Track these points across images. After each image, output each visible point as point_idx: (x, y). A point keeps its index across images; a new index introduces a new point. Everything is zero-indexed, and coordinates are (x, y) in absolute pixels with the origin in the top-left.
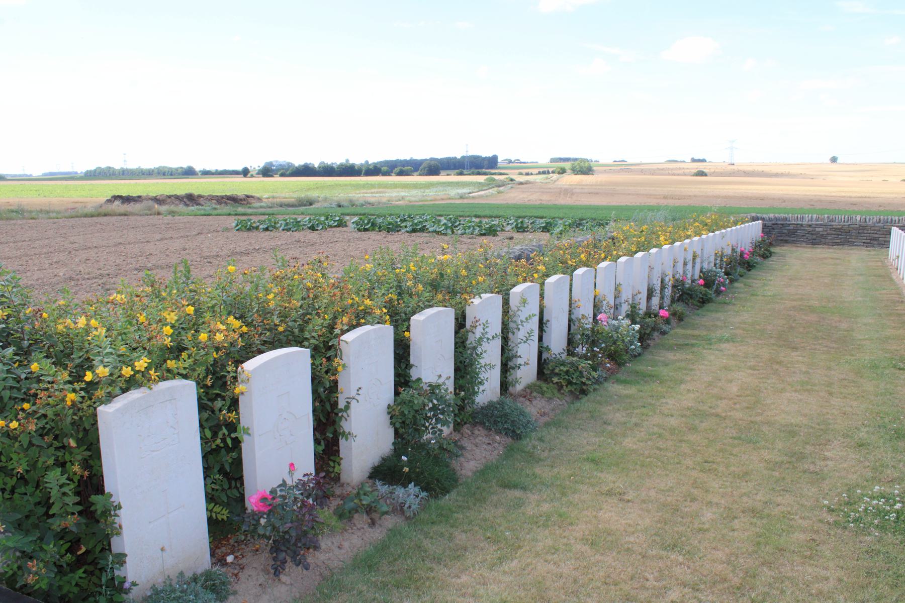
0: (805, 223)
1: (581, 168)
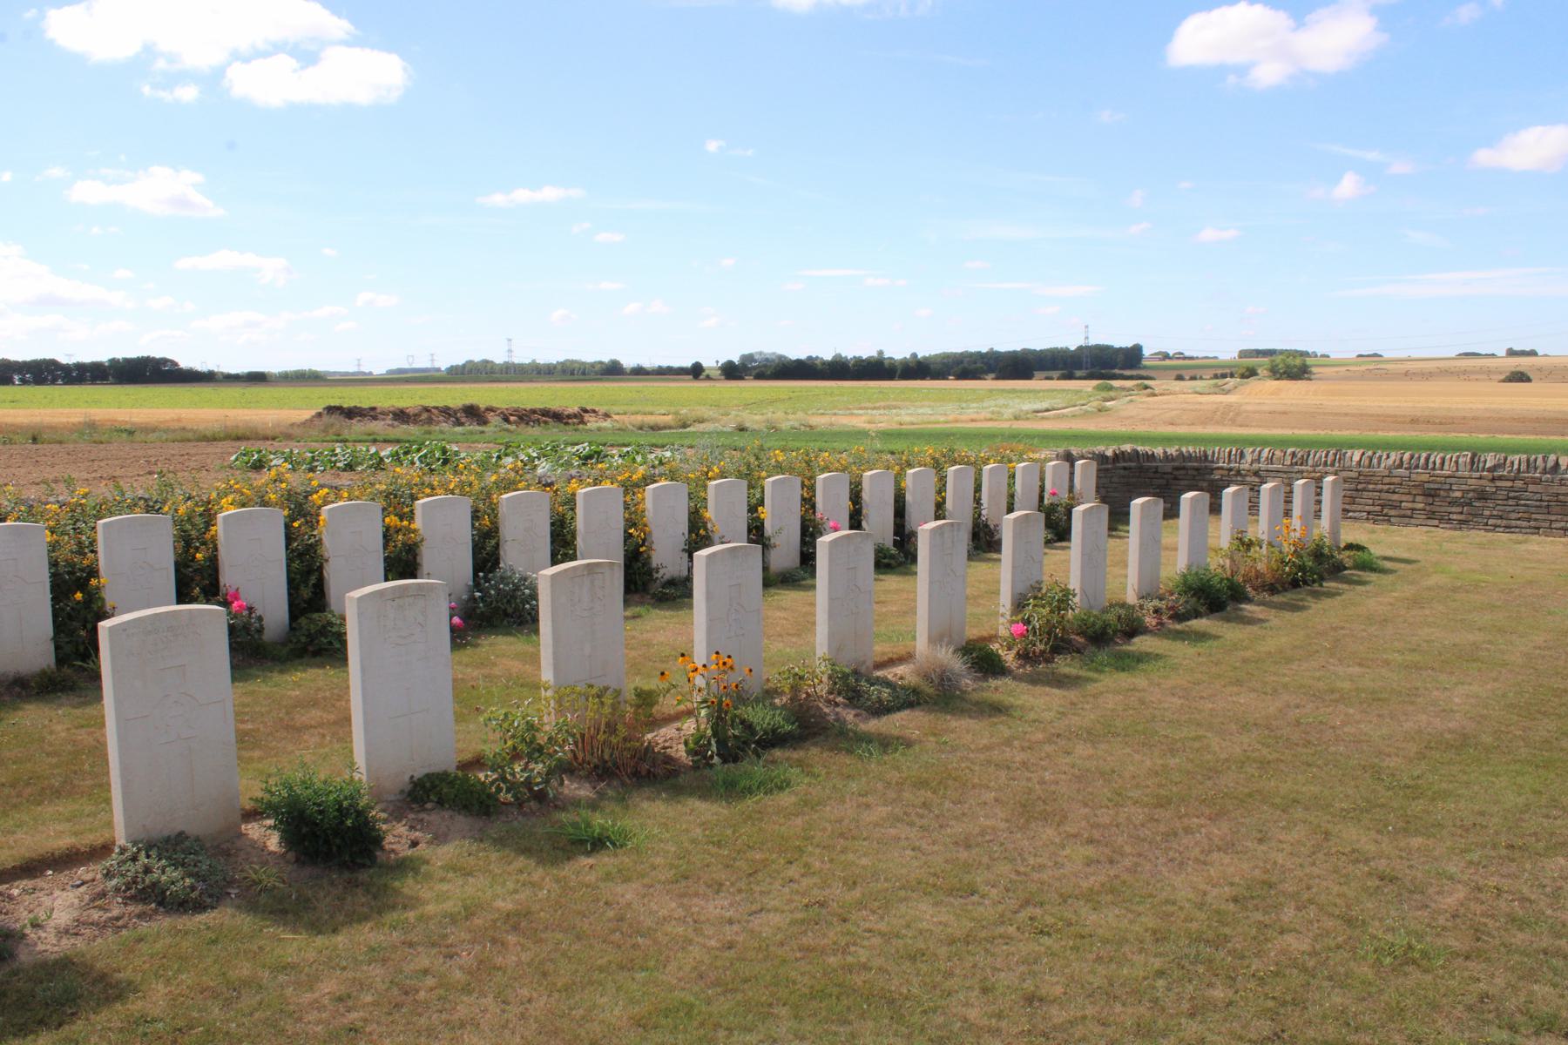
0: (1245, 466)
1: (1288, 367)
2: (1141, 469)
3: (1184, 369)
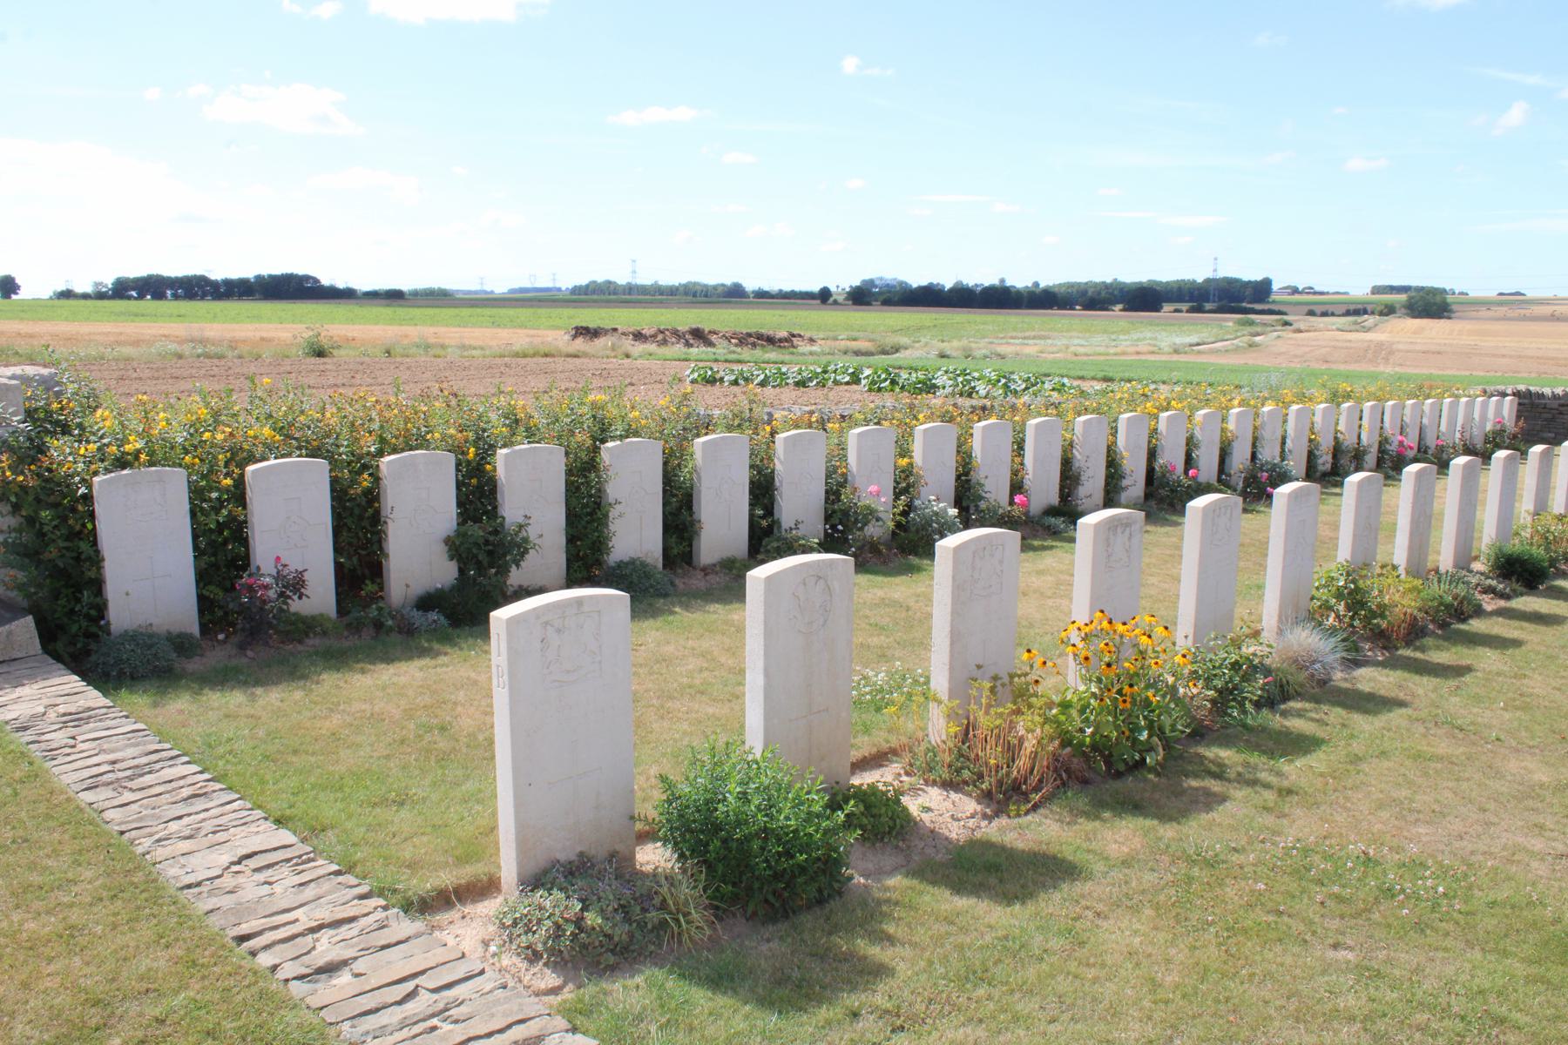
2: (1532, 405)
3: (1320, 307)
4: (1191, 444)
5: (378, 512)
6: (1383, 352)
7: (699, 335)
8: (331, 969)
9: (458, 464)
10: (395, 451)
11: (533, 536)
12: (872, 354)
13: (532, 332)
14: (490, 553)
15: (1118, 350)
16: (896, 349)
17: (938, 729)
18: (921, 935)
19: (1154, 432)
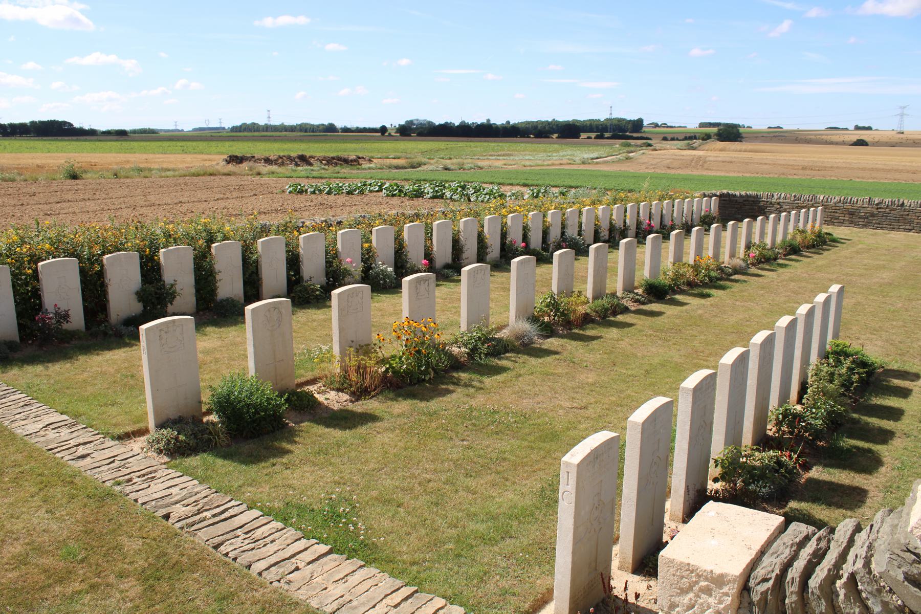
2: (730, 200)
3: (671, 135)
4: (526, 229)
5: (103, 282)
6: (701, 162)
7: (304, 159)
8: (83, 457)
9: (141, 258)
10: (111, 252)
11: (178, 290)
12: (405, 168)
13: (206, 157)
14: (158, 298)
15: (550, 162)
16: (420, 165)
17: (336, 368)
18: (309, 441)
19: (504, 225)
